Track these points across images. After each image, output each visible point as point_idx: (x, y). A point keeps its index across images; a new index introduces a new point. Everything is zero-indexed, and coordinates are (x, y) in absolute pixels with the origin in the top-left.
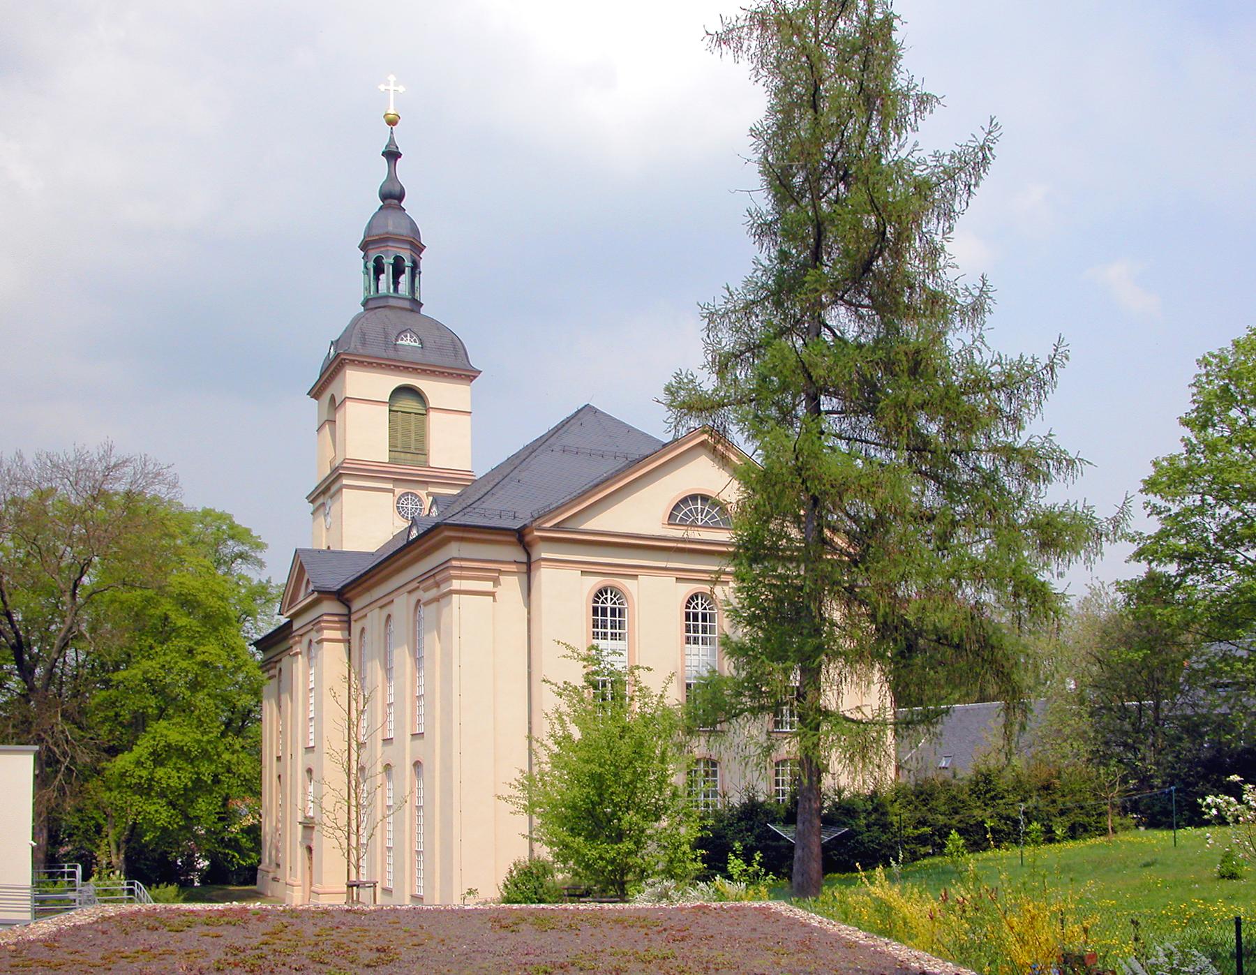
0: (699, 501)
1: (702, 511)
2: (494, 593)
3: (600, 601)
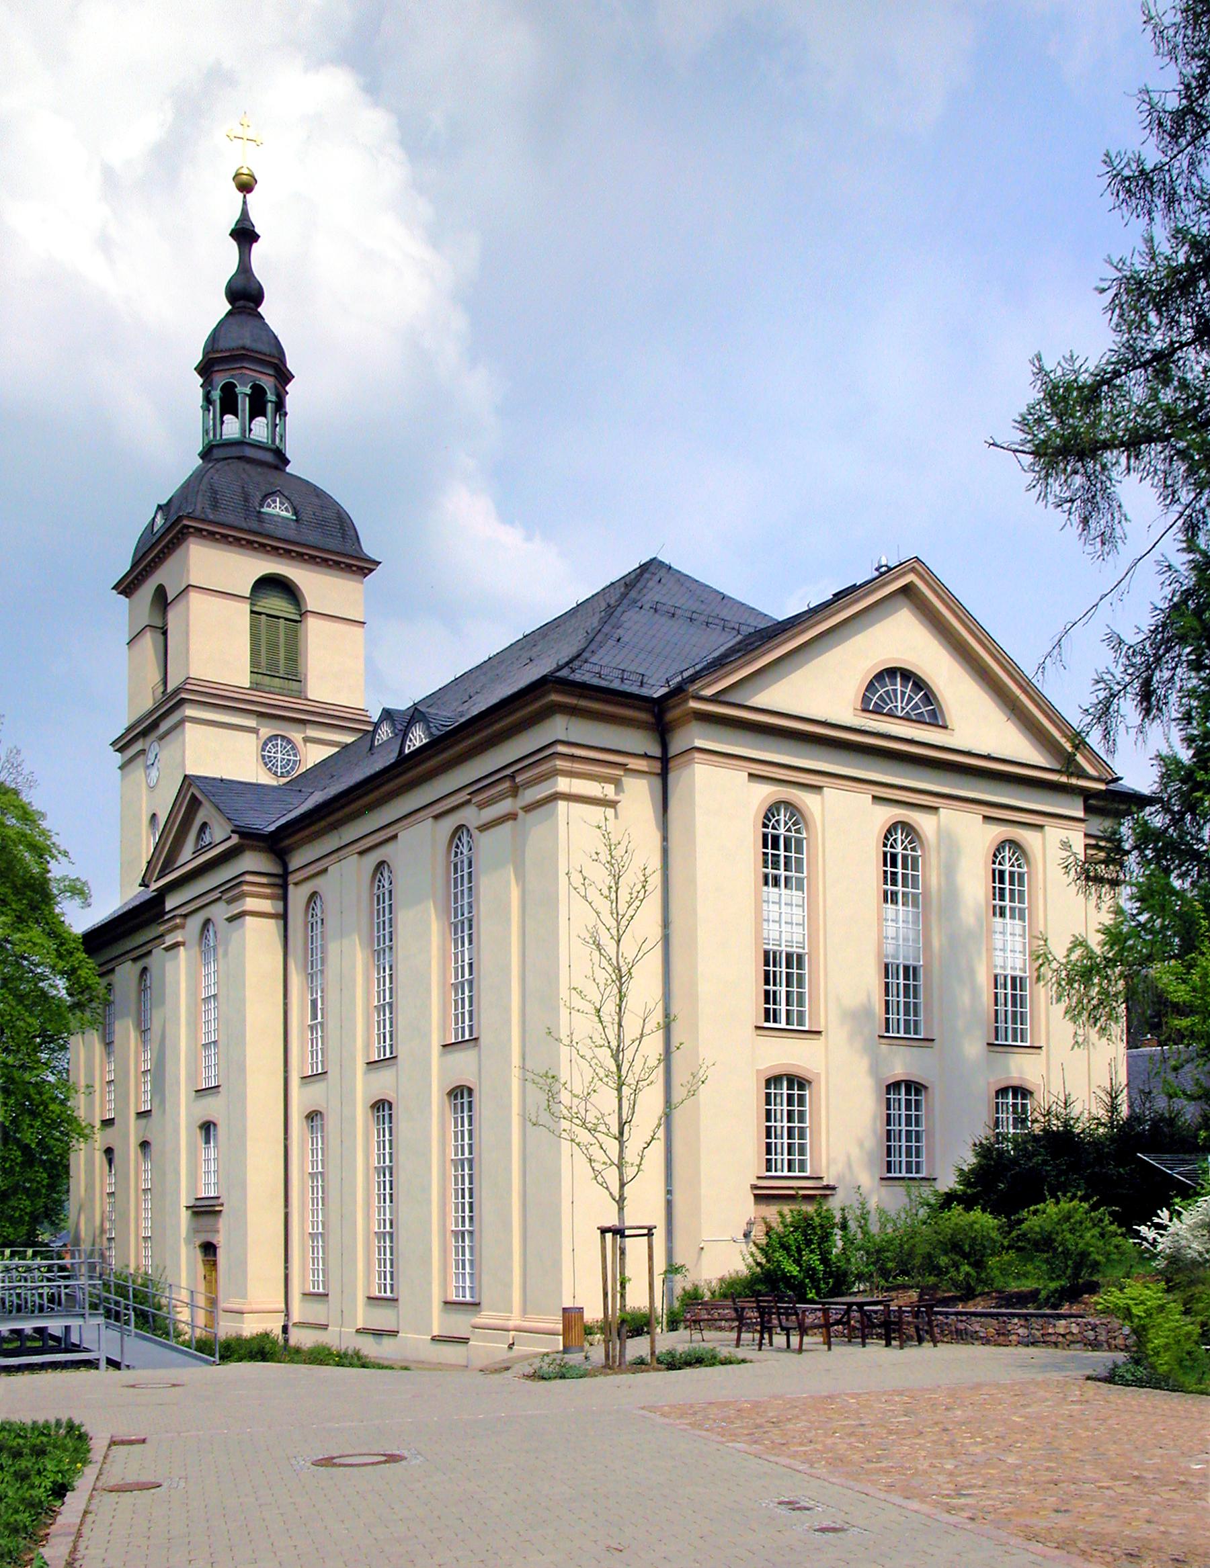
0: (899, 679)
2: (617, 802)
3: (771, 824)
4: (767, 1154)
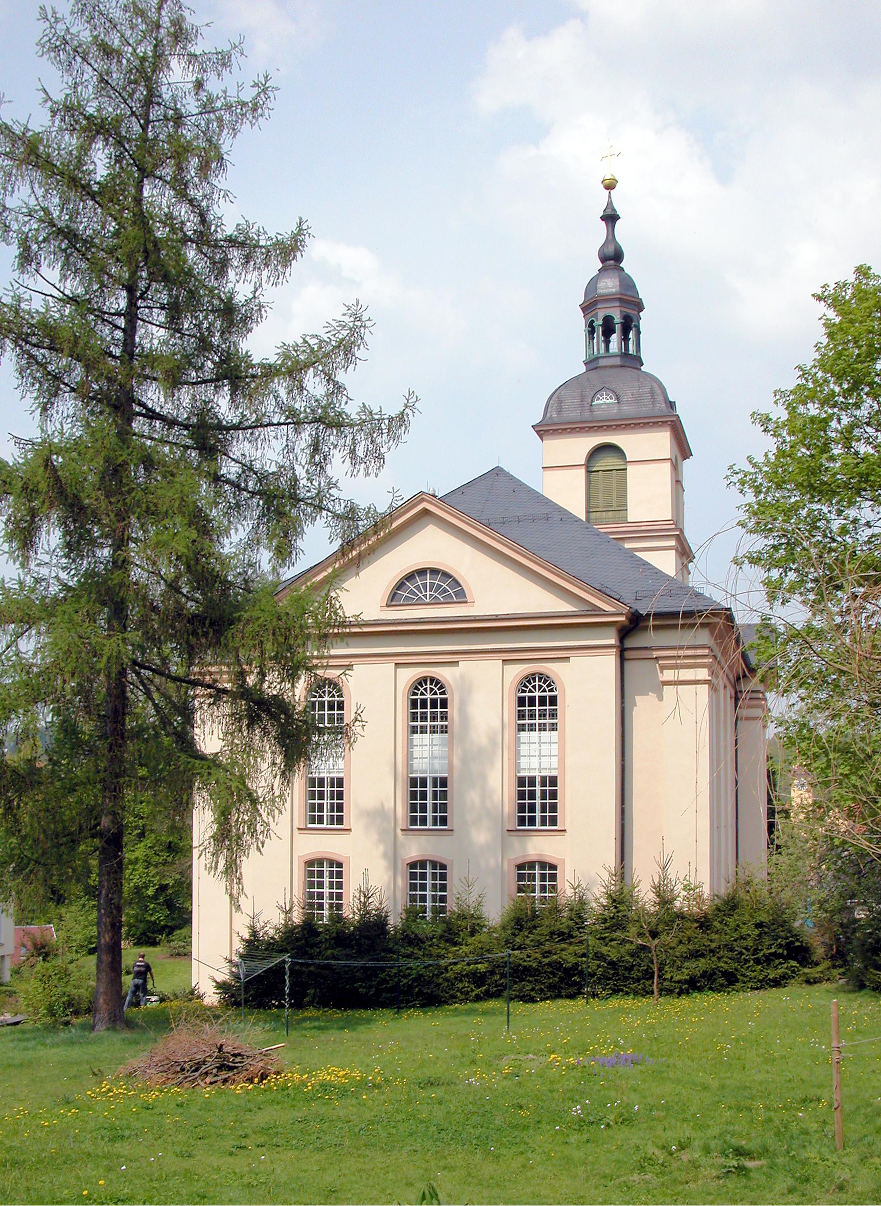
1: (425, 585)
4: (343, 702)
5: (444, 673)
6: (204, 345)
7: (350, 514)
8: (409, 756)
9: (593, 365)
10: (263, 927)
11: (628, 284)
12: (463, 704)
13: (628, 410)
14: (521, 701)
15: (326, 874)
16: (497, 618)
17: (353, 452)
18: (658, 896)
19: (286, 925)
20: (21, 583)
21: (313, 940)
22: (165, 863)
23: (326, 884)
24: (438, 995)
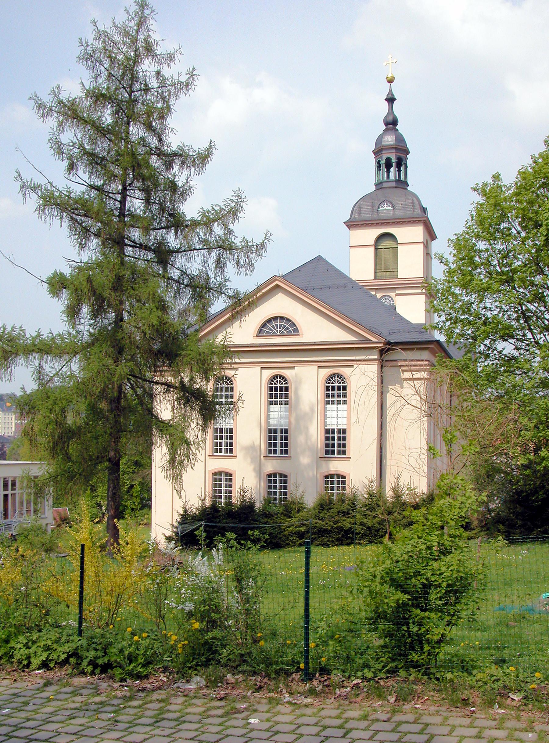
5: (286, 373)
6: (162, 209)
7: (236, 295)
8: (268, 417)
9: (380, 186)
10: (190, 508)
11: (400, 139)
12: (296, 390)
13: (399, 213)
14: (327, 388)
15: (223, 480)
16: (315, 344)
17: (238, 263)
18: (395, 494)
19: (202, 507)
20: (70, 334)
21: (216, 514)
22: (134, 472)
23: (223, 485)
24: (280, 543)
